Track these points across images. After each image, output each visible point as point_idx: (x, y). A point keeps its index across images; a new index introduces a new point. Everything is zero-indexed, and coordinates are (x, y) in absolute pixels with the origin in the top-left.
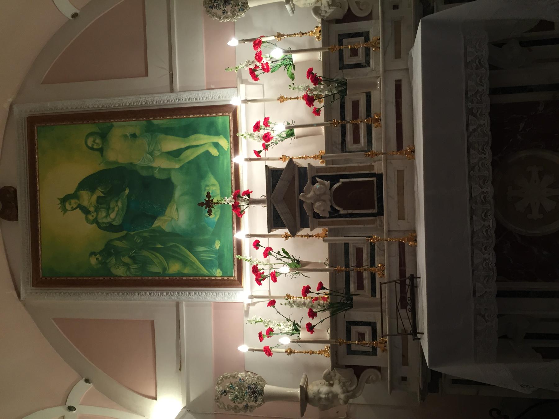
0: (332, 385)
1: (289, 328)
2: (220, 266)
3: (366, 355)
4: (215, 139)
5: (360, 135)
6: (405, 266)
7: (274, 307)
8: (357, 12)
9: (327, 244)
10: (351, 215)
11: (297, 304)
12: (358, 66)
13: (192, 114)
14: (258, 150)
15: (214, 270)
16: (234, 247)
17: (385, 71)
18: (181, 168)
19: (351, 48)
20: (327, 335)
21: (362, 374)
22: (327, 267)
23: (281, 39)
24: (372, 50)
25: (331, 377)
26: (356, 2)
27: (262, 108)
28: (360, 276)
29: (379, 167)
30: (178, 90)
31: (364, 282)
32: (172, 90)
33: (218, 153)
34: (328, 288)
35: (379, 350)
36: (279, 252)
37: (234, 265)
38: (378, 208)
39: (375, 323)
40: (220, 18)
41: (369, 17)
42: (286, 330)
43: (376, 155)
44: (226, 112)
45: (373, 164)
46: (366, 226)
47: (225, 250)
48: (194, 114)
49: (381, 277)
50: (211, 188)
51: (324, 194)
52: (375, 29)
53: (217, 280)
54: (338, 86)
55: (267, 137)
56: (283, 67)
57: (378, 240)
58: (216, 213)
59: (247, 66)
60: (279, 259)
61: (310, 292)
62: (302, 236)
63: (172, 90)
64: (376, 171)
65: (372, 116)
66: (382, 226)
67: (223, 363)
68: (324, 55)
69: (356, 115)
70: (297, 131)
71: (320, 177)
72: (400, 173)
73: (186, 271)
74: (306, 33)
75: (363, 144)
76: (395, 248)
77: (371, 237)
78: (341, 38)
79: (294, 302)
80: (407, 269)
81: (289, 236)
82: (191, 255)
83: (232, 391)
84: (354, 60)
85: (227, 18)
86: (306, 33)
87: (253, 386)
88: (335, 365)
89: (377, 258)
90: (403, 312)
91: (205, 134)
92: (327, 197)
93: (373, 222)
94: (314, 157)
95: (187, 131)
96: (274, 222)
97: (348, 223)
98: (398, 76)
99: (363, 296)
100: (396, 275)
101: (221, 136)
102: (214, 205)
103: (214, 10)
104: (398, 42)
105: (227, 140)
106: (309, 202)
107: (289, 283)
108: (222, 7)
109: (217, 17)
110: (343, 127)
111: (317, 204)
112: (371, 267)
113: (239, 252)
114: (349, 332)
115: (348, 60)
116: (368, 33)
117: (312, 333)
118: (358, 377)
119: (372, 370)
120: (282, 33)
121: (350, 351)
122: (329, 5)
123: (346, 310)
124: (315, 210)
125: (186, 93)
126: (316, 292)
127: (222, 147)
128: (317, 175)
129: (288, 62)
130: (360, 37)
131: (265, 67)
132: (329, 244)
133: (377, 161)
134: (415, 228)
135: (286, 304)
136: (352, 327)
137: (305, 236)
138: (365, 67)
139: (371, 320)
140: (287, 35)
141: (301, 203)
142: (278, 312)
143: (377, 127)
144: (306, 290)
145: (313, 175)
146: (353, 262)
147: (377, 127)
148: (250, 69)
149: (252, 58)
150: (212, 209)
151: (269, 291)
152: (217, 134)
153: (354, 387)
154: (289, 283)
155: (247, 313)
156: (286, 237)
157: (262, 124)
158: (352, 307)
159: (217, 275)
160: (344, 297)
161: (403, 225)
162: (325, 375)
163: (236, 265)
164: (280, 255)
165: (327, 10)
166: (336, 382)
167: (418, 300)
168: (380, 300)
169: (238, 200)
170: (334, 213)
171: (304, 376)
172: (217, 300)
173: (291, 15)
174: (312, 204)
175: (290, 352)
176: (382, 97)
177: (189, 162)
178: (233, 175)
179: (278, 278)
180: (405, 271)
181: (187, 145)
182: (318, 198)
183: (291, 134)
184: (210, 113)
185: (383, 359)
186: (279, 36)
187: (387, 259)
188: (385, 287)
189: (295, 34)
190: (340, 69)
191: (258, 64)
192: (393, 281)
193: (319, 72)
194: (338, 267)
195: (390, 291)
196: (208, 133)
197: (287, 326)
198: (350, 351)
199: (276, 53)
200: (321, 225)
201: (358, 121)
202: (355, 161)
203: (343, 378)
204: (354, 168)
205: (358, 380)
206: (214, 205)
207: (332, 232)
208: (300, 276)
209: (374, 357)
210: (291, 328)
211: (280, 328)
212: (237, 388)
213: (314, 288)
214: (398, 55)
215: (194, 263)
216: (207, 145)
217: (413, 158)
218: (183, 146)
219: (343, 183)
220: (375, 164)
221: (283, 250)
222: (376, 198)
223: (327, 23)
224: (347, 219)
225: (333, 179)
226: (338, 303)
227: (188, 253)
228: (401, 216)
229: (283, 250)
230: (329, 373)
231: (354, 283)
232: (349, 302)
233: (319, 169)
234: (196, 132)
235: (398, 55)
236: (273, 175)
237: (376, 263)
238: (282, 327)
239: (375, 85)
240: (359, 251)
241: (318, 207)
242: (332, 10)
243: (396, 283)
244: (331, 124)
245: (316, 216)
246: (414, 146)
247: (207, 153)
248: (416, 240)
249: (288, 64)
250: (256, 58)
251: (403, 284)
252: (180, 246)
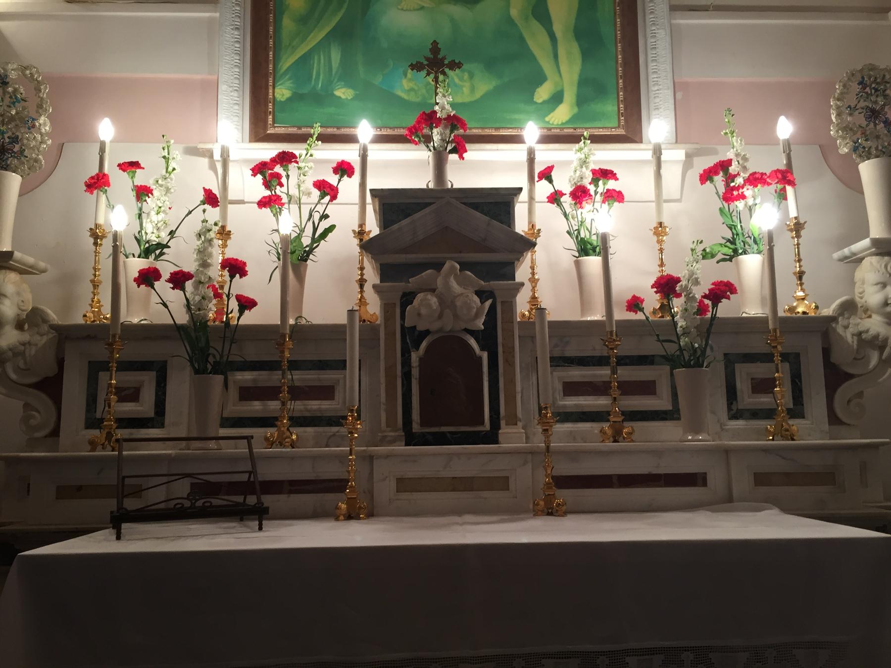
0: (19, 326)
1: (152, 235)
2: (297, 97)
3: (88, 405)
4: (570, 96)
5: (581, 398)
6: (290, 492)
7: (203, 203)
8: (844, 391)
9: (342, 319)
10: (407, 376)
11: (205, 249)
12: (732, 394)
13: (623, 48)
14: (554, 174)
15: (289, 84)
16: (338, 128)
17: (727, 452)
18: (510, 21)
19: (774, 379)
20: (133, 317)
21: (44, 396)
22: (292, 321)
23: (791, 230)
24: (769, 425)
25: (37, 326)
26: (862, 392)
27: (629, 204)
28: (270, 393)
29: (512, 437)
30: (674, 22)
31: (257, 403)
32: (674, 8)
33: (540, 101)
34: (242, 322)
35: (96, 432)
36: (327, 217)
37: (300, 128)
38: (423, 435)
39: (162, 425)
40: (838, 100)
41: (834, 419)
42: (149, 227)
43: (546, 430)
44: (626, 120)
45: (520, 424)
46: (383, 407)
47: (332, 110)
48: (624, 51)
49: (267, 439)
50: (467, 84)
51: (456, 316)
52: (811, 431)
53: (267, 89)
54: (695, 350)
55: (580, 194)
56: (729, 235)
57: (351, 433)
58: (412, 93)
59: (737, 155)
60: (311, 216)
61: (232, 276)
62: (362, 269)
63: (674, 8)
64: (505, 430)
65: (626, 424)
66: (383, 441)
67: (78, 94)
68: (763, 321)
69: (629, 388)
70: (593, 262)
71: (493, 308)
72: (501, 483)
73: (288, 24)
74: (801, 284)
75: (561, 403)
76: (331, 471)
77: (359, 418)
78: (793, 359)
79: (211, 240)
80: (283, 497)
81: (361, 240)
82: (323, 34)
83: (7, 100)
84: (743, 385)
85: (839, 115)
86: (801, 284)
87: (17, 148)
88: (67, 336)
89: (310, 431)
90: (182, 488)
91: (580, 76)
92: (448, 324)
93: (391, 423)
94: (534, 298)
95: (587, 36)
96: (393, 205)
97: (390, 370)
98: (716, 479)
99: (221, 395)
100: (267, 472)
101: (576, 110)
102: (432, 76)
103: (856, 88)
104: (789, 478)
105: (567, 122)
106: (440, 282)
107: (256, 233)
108: (863, 104)
109: (842, 93)
110: (600, 361)
111: (433, 300)
112: (291, 419)
113: (325, 139)
114: (143, 366)
115: (744, 374)
116: (802, 416)
117: (135, 280)
118: (38, 386)
119: (54, 419)
120: (803, 233)
121: (96, 368)
122: (860, 334)
123: (191, 361)
124: (420, 296)
125: (668, 38)
126: (234, 292)
127: (553, 110)
128: (498, 303)
129: (739, 244)
130: (794, 398)
131: (735, 193)
132: (344, 326)
133: (526, 433)
134: (379, 515)
135: (205, 221)
136: (153, 374)
137: (362, 275)
138: (729, 409)
139: (169, 417)
140: (798, 244)
141: (438, 266)
142: (190, 212)
143: (602, 431)
144: (236, 268)
145: (497, 293)
146: (299, 377)
147: (602, 431)
148: (729, 162)
149: (754, 167)
150: (424, 73)
151: (242, 202)
152: (581, 101)
153: (13, 376)
154: (256, 233)
155: (193, 151)
156: (360, 233)
157: (611, 184)
158: (197, 372)
159: (277, 90)
160: (221, 356)
161: (385, 489)
162: (42, 311)
163: (299, 132)
164: (320, 220)
165: (851, 330)
166: (25, 337)
167: (209, 523)
168: (213, 435)
169: (446, 127)
170: (412, 337)
171: (42, 265)
172: (223, 87)
173: (836, 255)
174: (433, 291)
175: (97, 235)
176: (667, 442)
177: (522, 39)
178: (494, 133)
179: (266, 211)
180: (280, 493)
181: (559, 34)
182: (447, 303)
183: (584, 248)
184: (625, 87)
185: (76, 439)
186: (798, 227)
187: (303, 451)
188: (242, 449)
189: (799, 261)
190: (725, 355)
191: (739, 181)
192: (254, 465)
193: (725, 309)
194: (289, 344)
195: (234, 459)
196: (583, 82)
197: (158, 229)
198: (96, 368)
199: (764, 214)
200: (387, 308)
201: (616, 393)
202: (531, 386)
203: (33, 352)
204: (511, 382)
205: (29, 386)
206: (432, 76)
207: (369, 331)
208: (272, 262)
209: (82, 424)
210: (154, 239)
211: (153, 213)
212: (13, 112)
213: (241, 286)
214: (761, 479)
215: (304, 39)
216: (557, 79)
217: (537, 512)
218: (558, 28)
219: (480, 358)
220: (519, 429)
221: (332, 228)
222: (444, 429)
223: (821, 329)
224: (399, 367)
225: (488, 338)
226: (207, 342)
227: (328, 29)
228: (404, 485)
229: (332, 228)
230: (45, 321)
231: (254, 380)
232: (209, 367)
233: (510, 306)
234: (586, 55)
235: (761, 479)
236: (499, 203)
237: (301, 430)
238: (155, 218)
239: (696, 430)
240: (326, 392)
241: (426, 305)
242: (849, 338)
243: (250, 473)
244: (611, 332)
245: (407, 298)
246: (565, 514)
247: (539, 79)
248: (349, 517)
249: (735, 247)
250: (755, 173)
251: (247, 488)
252: (343, 11)
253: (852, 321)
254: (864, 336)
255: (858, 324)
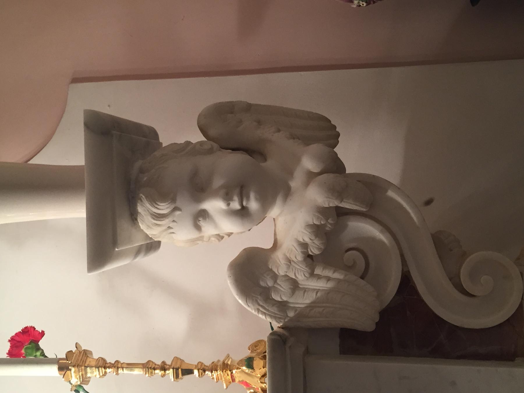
122: (310, 259)
253: (281, 272)
254: (314, 251)
255: (289, 261)
